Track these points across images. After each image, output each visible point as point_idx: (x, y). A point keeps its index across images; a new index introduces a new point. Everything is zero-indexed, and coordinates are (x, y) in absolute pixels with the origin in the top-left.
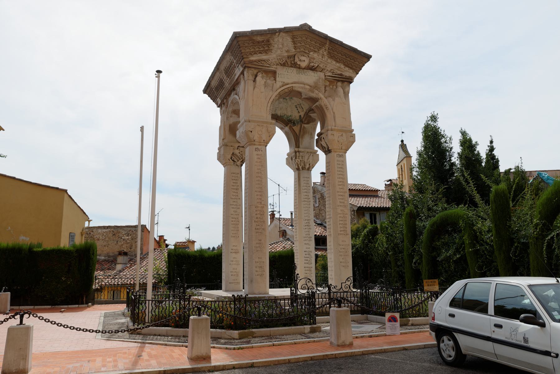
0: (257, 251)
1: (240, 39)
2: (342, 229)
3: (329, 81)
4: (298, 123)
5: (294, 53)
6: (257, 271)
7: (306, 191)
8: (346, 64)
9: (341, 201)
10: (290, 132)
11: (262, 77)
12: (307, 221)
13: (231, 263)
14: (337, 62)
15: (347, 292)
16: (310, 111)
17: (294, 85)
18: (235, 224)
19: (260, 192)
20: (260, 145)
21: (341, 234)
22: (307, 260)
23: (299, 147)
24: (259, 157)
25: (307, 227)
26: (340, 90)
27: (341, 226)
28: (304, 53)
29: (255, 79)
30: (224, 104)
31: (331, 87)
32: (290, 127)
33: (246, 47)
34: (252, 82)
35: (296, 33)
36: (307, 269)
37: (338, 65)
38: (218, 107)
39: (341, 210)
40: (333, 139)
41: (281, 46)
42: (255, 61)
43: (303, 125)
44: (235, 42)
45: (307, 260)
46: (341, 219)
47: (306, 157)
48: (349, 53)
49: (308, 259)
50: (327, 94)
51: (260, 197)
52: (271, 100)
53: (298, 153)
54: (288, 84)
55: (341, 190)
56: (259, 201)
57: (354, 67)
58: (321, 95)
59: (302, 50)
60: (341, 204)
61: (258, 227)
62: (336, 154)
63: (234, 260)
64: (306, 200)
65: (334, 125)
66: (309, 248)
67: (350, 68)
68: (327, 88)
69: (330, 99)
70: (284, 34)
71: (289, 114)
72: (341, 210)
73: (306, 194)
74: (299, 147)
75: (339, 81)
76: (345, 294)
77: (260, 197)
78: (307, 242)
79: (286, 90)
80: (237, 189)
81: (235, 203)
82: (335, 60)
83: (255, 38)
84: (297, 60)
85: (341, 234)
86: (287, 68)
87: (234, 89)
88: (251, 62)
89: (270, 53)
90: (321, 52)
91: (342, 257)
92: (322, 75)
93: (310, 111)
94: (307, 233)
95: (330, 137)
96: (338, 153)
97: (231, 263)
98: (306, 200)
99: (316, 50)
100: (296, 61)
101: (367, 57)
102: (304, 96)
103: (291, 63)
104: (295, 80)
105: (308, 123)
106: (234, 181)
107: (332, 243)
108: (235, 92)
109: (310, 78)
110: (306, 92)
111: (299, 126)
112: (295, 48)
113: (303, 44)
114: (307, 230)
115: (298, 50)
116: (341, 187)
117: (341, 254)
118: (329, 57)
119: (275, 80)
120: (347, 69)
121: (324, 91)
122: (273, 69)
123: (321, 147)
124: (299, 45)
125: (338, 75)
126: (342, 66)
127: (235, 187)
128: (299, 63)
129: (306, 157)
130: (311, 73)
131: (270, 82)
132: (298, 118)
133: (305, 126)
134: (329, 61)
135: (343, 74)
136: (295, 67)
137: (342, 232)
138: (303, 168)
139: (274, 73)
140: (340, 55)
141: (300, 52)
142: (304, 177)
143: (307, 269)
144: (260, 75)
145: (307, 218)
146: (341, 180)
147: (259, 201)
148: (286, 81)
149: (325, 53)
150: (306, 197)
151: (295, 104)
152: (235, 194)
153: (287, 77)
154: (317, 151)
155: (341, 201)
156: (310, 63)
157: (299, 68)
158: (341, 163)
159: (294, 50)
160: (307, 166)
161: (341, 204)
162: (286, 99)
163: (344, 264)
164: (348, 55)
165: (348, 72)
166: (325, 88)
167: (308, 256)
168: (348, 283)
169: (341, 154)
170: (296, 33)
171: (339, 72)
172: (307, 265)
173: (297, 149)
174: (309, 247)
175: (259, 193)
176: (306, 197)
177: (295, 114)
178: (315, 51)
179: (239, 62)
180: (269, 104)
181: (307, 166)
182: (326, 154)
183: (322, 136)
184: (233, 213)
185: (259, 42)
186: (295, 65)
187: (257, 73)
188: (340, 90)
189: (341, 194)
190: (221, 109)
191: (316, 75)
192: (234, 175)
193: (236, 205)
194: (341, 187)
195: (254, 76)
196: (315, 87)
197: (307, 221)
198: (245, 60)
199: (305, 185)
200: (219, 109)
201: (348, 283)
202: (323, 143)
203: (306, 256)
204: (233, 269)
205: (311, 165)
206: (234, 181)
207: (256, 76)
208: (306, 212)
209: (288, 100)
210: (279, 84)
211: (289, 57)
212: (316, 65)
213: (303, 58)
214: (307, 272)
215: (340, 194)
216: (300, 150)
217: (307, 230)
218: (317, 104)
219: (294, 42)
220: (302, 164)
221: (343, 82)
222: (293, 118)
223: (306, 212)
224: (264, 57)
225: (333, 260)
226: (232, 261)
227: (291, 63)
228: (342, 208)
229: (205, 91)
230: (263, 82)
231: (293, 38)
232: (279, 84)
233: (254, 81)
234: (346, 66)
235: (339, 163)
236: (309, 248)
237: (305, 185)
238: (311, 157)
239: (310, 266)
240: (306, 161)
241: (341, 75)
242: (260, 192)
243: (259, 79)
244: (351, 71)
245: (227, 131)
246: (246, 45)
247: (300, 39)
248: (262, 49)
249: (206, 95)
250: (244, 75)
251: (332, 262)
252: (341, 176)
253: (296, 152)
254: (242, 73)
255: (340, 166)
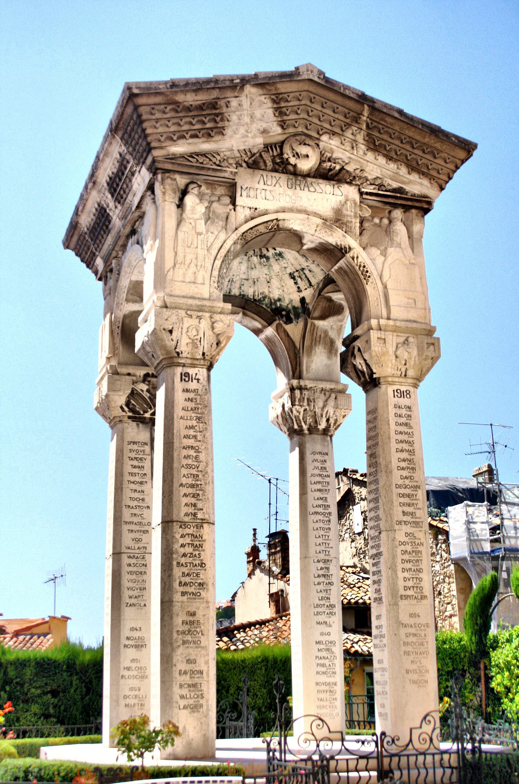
0: (184, 642)
1: (141, 101)
2: (410, 584)
3: (369, 206)
4: (297, 316)
5: (281, 138)
6: (182, 697)
7: (319, 486)
8: (414, 163)
9: (407, 509)
10: (277, 339)
11: (201, 196)
12: (321, 565)
13: (126, 673)
14: (390, 158)
15: (424, 754)
16: (325, 286)
17: (281, 216)
18: (136, 573)
19: (192, 486)
20: (193, 366)
21: (407, 597)
22: (323, 665)
23: (300, 377)
24: (191, 395)
25: (322, 579)
26: (400, 228)
27: (406, 575)
28: (305, 138)
29: (181, 200)
30: (111, 271)
31: (377, 221)
32: (278, 329)
33: (157, 120)
34: (174, 207)
35: (284, 87)
36: (323, 688)
37: (392, 166)
38: (100, 279)
39: (407, 534)
40: (384, 354)
41: (247, 119)
42: (182, 156)
43: (310, 321)
44: (129, 110)
45: (323, 665)
46: (406, 557)
47: (320, 403)
48: (418, 138)
49: (327, 662)
50: (365, 238)
51: (193, 501)
52: (223, 252)
53: (297, 392)
54: (265, 213)
55: (407, 482)
56: (191, 510)
57: (434, 173)
58: (350, 241)
59: (300, 129)
60: (405, 518)
61: (187, 579)
62: (390, 390)
63: (134, 665)
64: (320, 510)
65: (385, 314)
66: (329, 634)
67: (423, 174)
68: (366, 225)
69: (375, 252)
70: (254, 90)
71: (275, 294)
72: (407, 534)
73: (318, 494)
74: (300, 377)
75: (395, 206)
76: (421, 758)
77: (193, 501)
78: (322, 618)
79: (262, 229)
80: (141, 483)
81: (136, 520)
82: (385, 156)
83: (180, 98)
84: (288, 153)
85: (407, 597)
86: (265, 173)
87: (133, 232)
88: (173, 158)
89: (217, 138)
90: (348, 134)
91: (411, 658)
92: (350, 192)
93: (325, 286)
94: (323, 594)
95: (376, 347)
96: (395, 387)
97: (126, 673)
98: (320, 510)
99: (338, 130)
100: (285, 156)
101: (468, 148)
102: (308, 244)
103: (274, 162)
104: (284, 202)
105: (323, 317)
106: (135, 463)
107: (383, 621)
108: (134, 238)
109: (326, 198)
110: (314, 234)
111: (301, 324)
112: (283, 125)
113: (304, 115)
114: (321, 587)
115: (291, 130)
116: (405, 473)
117: (409, 648)
118: (369, 149)
119: (233, 202)
120: (415, 177)
121: (358, 231)
122: (226, 175)
123: (353, 374)
124: (293, 116)
125: (394, 190)
126: (403, 170)
127: (137, 479)
128: (292, 161)
129: (320, 403)
130: (326, 187)
131: (221, 208)
132: (297, 304)
133: (320, 323)
134: (370, 156)
135: (407, 188)
136: (285, 171)
137: (410, 593)
138: (312, 430)
139: (232, 190)
140: (397, 142)
141: (295, 135)
142: (314, 453)
143: (323, 688)
144: (194, 191)
145: (322, 556)
146: (405, 455)
147: (191, 510)
148: (262, 205)
149: (360, 138)
150: (320, 502)
151: (289, 271)
152: (136, 495)
153: (266, 197)
154: (346, 387)
155: (407, 509)
156: (322, 162)
157: (295, 174)
158: (404, 412)
159: (279, 130)
160: (323, 425)
161: (405, 518)
162: (268, 258)
163: (415, 677)
164: (417, 141)
165: (417, 185)
166: (361, 223)
167: (324, 654)
168: (427, 728)
169: (403, 388)
170: (284, 87)
171: (395, 185)
172: (323, 679)
173: (295, 382)
174: (326, 630)
175: (190, 491)
176: (320, 502)
177: (288, 294)
178: (334, 134)
179: (141, 161)
180: (218, 263)
181: (323, 425)
182: (366, 391)
183: (358, 343)
184: (132, 544)
185: (189, 109)
186: (282, 166)
187: (187, 186)
188: (400, 228)
189: (407, 491)
190: (105, 284)
191: (337, 191)
192: (135, 447)
193: (140, 523)
194: (405, 473)
195: (178, 195)
196: (338, 220)
197: (321, 565)
198: (156, 153)
199: (317, 472)
200: (101, 283)
201: (427, 728)
202: (359, 362)
203: (320, 654)
204: (131, 689)
205: (332, 421)
206: (135, 463)
207: (184, 193)
208: (320, 541)
209: (272, 260)
210: (242, 213)
211: (268, 147)
212: (338, 167)
213: (303, 150)
214: (322, 696)
215: (402, 491)
216: (302, 383)
217: (321, 587)
218: (342, 263)
219: (279, 112)
220: (309, 420)
221: (406, 208)
222: (285, 303)
223: (320, 541)
224: (204, 146)
225: (386, 664)
226: (128, 669)
227: (273, 160)
228: (408, 529)
229: (67, 245)
230: (201, 209)
231: (277, 100)
232: (242, 213)
233: (180, 205)
234: (413, 168)
235: (399, 412)
236: (329, 634)
237: (317, 472)
238: (331, 402)
239: (332, 680)
240: (318, 411)
241: (400, 190)
242: (192, 486)
243: (190, 200)
244: (425, 182)
245: (118, 339)
246: (158, 115)
247: (297, 103)
248: (198, 126)
249: (70, 254)
250: (153, 193)
251: (383, 670)
252: (405, 446)
253: (292, 389)
254: (151, 188)
255: (403, 420)
